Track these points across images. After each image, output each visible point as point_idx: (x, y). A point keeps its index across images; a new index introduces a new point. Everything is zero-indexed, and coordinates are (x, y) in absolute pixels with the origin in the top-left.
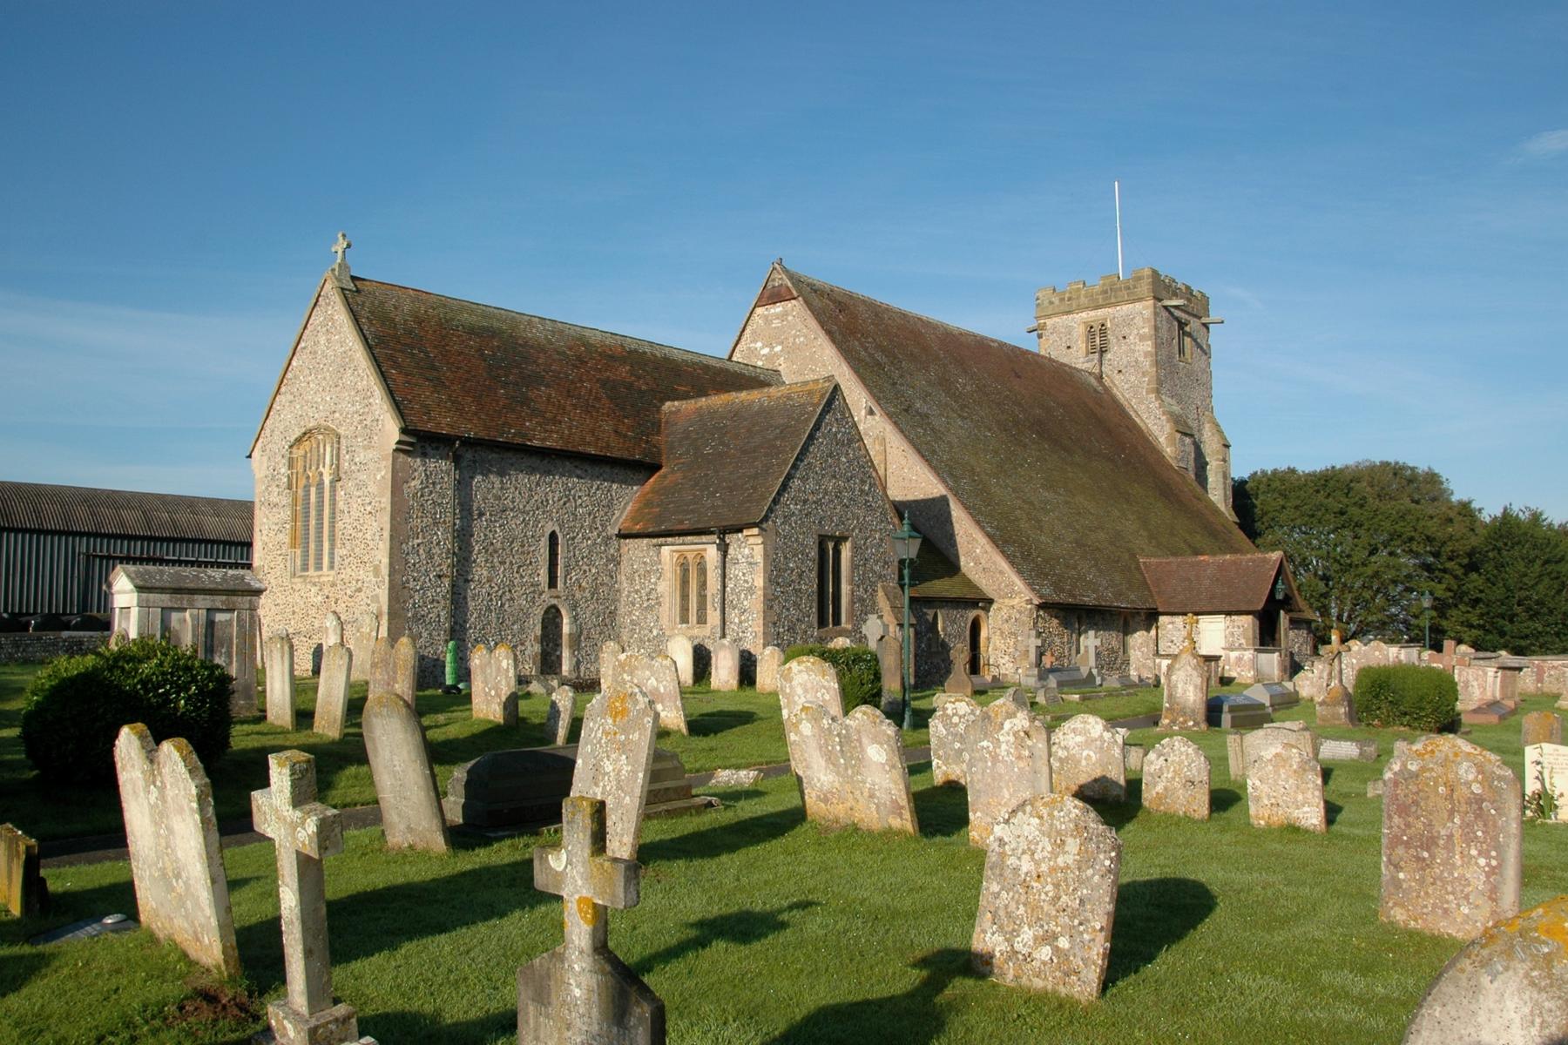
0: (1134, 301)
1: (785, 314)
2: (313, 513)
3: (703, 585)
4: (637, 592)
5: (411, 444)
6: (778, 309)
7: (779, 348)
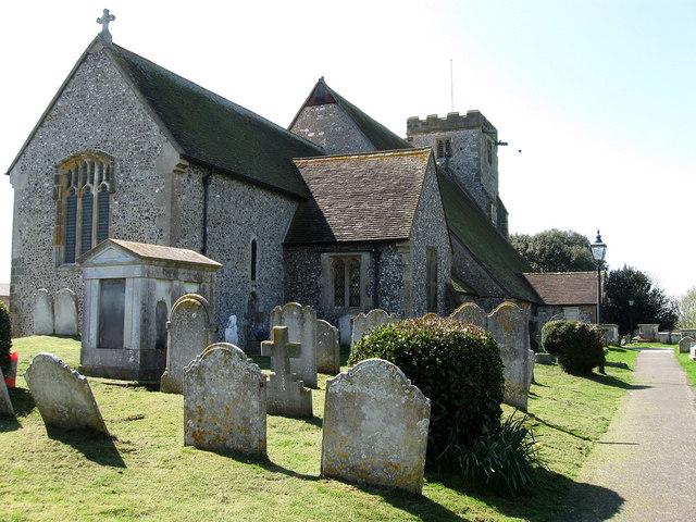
0: (468, 128)
6: (322, 108)
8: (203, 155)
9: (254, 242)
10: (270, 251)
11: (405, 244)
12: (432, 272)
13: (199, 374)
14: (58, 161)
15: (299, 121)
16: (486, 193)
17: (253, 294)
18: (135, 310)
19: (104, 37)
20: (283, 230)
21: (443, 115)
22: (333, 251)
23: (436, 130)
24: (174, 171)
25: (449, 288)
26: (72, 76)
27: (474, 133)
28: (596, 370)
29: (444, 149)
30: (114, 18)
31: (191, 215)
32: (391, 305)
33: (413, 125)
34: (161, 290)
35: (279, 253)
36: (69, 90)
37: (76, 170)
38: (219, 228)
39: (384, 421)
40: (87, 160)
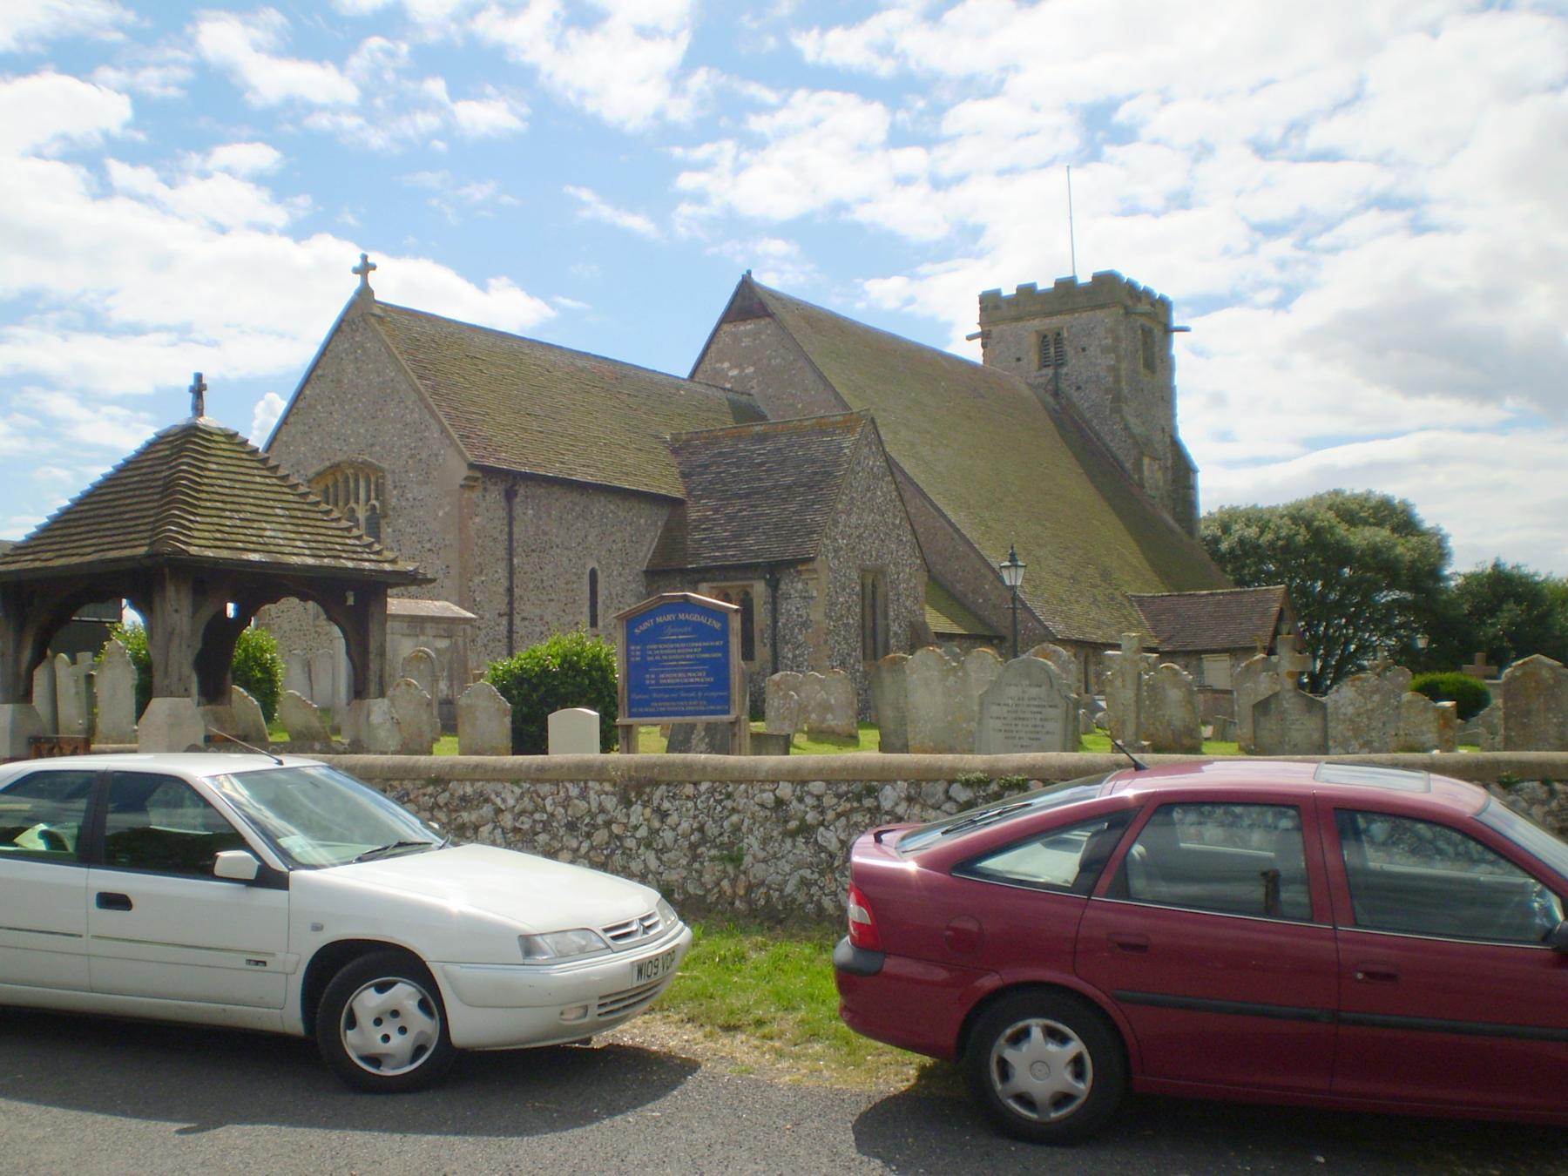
0: (1093, 308)
5: (476, 479)
6: (749, 326)
7: (750, 370)
8: (505, 460)
9: (593, 573)
11: (810, 566)
14: (311, 472)
15: (713, 348)
19: (365, 293)
23: (1034, 315)
27: (1106, 318)
29: (1052, 349)
32: (795, 657)
37: (336, 485)
40: (350, 471)
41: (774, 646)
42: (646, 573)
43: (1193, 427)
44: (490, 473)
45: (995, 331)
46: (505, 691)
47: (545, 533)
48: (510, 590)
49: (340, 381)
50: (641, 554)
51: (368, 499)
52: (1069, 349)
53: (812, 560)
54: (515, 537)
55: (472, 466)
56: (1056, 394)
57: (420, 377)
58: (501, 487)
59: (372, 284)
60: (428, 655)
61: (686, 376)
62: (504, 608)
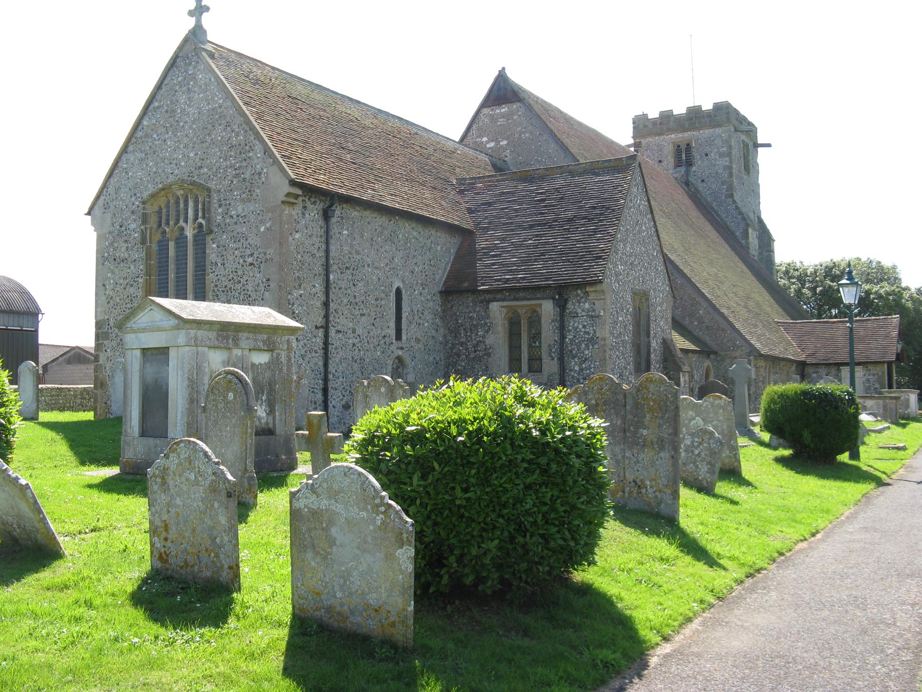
1: (507, 116)
2: (172, 267)
3: (536, 337)
4: (462, 344)
5: (297, 197)
6: (504, 109)
8: (321, 181)
9: (398, 292)
10: (422, 305)
11: (599, 287)
12: (642, 322)
13: (163, 478)
14: (146, 195)
16: (741, 213)
17: (399, 358)
18: (179, 388)
19: (196, 36)
20: (441, 275)
21: (680, 109)
22: (503, 300)
23: (670, 130)
24: (283, 202)
25: (667, 345)
26: (159, 87)
28: (844, 457)
29: (684, 156)
30: (207, 9)
31: (308, 258)
32: (581, 370)
33: (642, 126)
34: (216, 360)
35: (435, 304)
36: (156, 104)
37: (168, 206)
38: (348, 274)
39: (358, 548)
40: (180, 193)
41: (561, 360)
42: (441, 292)
43: (772, 211)
44: (311, 191)
45: (644, 141)
46: (393, 479)
47: (358, 253)
48: (326, 304)
49: (173, 111)
50: (437, 277)
51: (196, 218)
52: (696, 154)
53: (601, 282)
54: (332, 254)
55: (293, 183)
56: (687, 183)
57: (246, 104)
58: (320, 206)
59: (205, 26)
60: (240, 379)
61: (457, 139)
62: (320, 321)
